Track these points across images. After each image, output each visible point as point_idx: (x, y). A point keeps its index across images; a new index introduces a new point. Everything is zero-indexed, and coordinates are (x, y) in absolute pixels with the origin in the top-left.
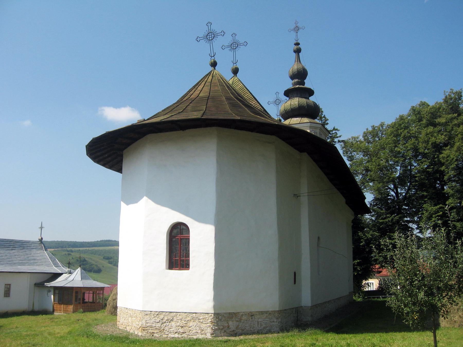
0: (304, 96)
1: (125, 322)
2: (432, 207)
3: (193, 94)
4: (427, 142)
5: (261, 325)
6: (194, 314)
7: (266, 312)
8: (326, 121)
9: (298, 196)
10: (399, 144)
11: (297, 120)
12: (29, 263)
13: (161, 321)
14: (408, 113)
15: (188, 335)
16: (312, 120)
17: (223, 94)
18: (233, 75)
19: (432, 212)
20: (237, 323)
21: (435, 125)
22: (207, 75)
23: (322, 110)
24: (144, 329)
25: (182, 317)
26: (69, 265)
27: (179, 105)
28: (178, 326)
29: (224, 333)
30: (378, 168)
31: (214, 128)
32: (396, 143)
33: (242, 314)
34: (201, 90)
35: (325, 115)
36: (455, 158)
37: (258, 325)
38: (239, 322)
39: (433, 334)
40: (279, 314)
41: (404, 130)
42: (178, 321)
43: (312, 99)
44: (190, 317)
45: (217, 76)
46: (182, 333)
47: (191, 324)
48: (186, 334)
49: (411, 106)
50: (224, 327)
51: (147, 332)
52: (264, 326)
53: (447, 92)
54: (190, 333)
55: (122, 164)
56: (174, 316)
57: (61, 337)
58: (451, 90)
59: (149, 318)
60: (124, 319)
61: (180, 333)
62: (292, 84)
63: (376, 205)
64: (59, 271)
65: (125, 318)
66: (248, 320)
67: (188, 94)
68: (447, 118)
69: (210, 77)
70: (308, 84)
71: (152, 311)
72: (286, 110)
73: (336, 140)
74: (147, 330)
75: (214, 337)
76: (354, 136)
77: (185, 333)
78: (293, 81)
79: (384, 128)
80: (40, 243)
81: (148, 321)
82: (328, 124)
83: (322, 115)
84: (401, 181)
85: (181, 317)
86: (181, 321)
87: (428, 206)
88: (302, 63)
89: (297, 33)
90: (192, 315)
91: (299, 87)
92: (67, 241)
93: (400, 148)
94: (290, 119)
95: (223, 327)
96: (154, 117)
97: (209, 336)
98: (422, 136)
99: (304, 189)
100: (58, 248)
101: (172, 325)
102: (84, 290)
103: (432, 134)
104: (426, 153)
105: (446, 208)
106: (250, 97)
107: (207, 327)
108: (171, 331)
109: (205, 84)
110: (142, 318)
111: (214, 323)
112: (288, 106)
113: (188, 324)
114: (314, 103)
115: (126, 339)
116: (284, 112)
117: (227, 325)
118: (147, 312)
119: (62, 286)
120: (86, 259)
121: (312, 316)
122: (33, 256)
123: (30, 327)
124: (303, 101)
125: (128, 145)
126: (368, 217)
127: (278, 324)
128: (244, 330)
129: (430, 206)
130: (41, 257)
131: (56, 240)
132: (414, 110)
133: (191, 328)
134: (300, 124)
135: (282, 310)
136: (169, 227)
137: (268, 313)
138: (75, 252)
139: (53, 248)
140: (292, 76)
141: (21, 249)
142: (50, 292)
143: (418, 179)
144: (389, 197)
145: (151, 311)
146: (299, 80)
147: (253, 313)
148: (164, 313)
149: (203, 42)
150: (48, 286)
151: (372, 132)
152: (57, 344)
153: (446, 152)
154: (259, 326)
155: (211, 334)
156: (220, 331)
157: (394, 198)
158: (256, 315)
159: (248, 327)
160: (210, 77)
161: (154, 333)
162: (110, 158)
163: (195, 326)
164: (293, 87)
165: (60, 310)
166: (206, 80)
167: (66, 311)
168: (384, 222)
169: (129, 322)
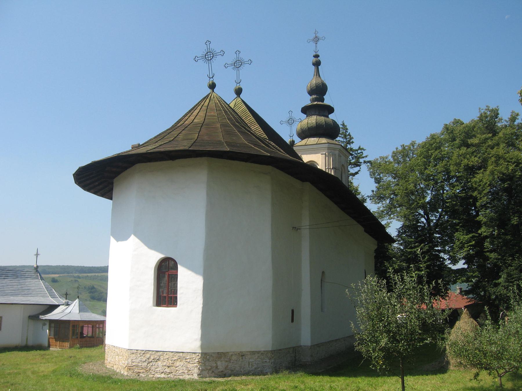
0: (323, 114)
1: (112, 360)
2: (464, 236)
3: (187, 119)
4: (458, 164)
5: (252, 366)
6: (182, 354)
7: (258, 352)
8: (351, 139)
9: (298, 229)
10: (429, 166)
11: (314, 140)
12: (23, 294)
13: (147, 360)
14: (441, 131)
15: (174, 375)
16: (330, 141)
17: (219, 120)
18: (236, 96)
19: (464, 241)
20: (226, 364)
21: (468, 146)
22: (205, 98)
23: (347, 127)
24: (129, 368)
25: (168, 356)
26: (66, 295)
27: (171, 132)
28: (165, 366)
29: (212, 373)
30: (406, 192)
31: (204, 158)
32: (426, 165)
33: (232, 354)
34: (197, 116)
35: (349, 133)
36: (489, 183)
37: (249, 365)
38: (229, 362)
39: (401, 379)
40: (273, 354)
41: (435, 151)
42: (165, 360)
43: (331, 116)
44: (177, 356)
45: (215, 99)
46: (169, 374)
47: (178, 363)
48: (172, 374)
49: (444, 124)
50: (212, 367)
51: (133, 371)
52: (255, 366)
53: (483, 109)
54: (176, 373)
55: (113, 192)
56: (161, 356)
57: (44, 376)
58: (487, 106)
59: (136, 357)
60: (112, 357)
61: (166, 373)
62: (310, 100)
63: (405, 232)
64: (56, 302)
65: (112, 356)
66: (238, 360)
67: (181, 120)
68: (481, 138)
69: (208, 101)
70: (328, 100)
71: (138, 350)
72: (303, 130)
73: (361, 160)
74: (133, 369)
75: (201, 377)
76: (383, 156)
77: (172, 373)
78: (312, 97)
79: (415, 147)
80: (35, 271)
81: (134, 360)
82: (353, 142)
83: (347, 133)
84: (433, 207)
85: (167, 357)
86: (167, 361)
87: (460, 234)
88: (321, 77)
89: (317, 43)
90: (179, 355)
91: (317, 104)
92: (73, 266)
93: (430, 170)
94: (307, 139)
95: (210, 367)
96: (145, 145)
97: (195, 377)
98: (455, 157)
99: (306, 222)
100: (63, 273)
101: (159, 365)
102: (83, 323)
103: (464, 156)
104: (458, 176)
105: (418, 252)
106: (253, 121)
107: (194, 367)
108: (157, 371)
109: (201, 108)
110: (128, 356)
111: (201, 363)
112: (305, 125)
113: (175, 364)
114: (333, 122)
115: (108, 378)
116: (300, 131)
117: (215, 365)
118: (133, 350)
119: (58, 319)
120: (95, 286)
121: (312, 356)
122: (27, 285)
123: (17, 364)
124: (322, 119)
125: (117, 174)
126: (396, 245)
127: (270, 365)
128: (233, 371)
129: (462, 235)
130: (36, 287)
131: (61, 265)
132: (447, 129)
133: (178, 368)
134: (317, 145)
135: (276, 350)
136: (159, 260)
137: (260, 353)
138: (83, 278)
139: (58, 274)
140: (310, 92)
141: (15, 278)
142: (45, 326)
143: (449, 204)
144: (419, 224)
145: (137, 350)
146: (317, 96)
147: (244, 353)
148: (150, 352)
149: (201, 62)
150: (42, 319)
151: (402, 151)
152: (37, 384)
153: (479, 176)
154: (250, 367)
155: (198, 375)
156: (207, 371)
157: (425, 226)
158: (247, 355)
159: (238, 368)
160: (208, 101)
161: (140, 373)
162: (101, 186)
163: (182, 366)
164: (311, 104)
165: (56, 346)
166: (202, 104)
167: (61, 347)
168: (412, 252)
169: (116, 361)
